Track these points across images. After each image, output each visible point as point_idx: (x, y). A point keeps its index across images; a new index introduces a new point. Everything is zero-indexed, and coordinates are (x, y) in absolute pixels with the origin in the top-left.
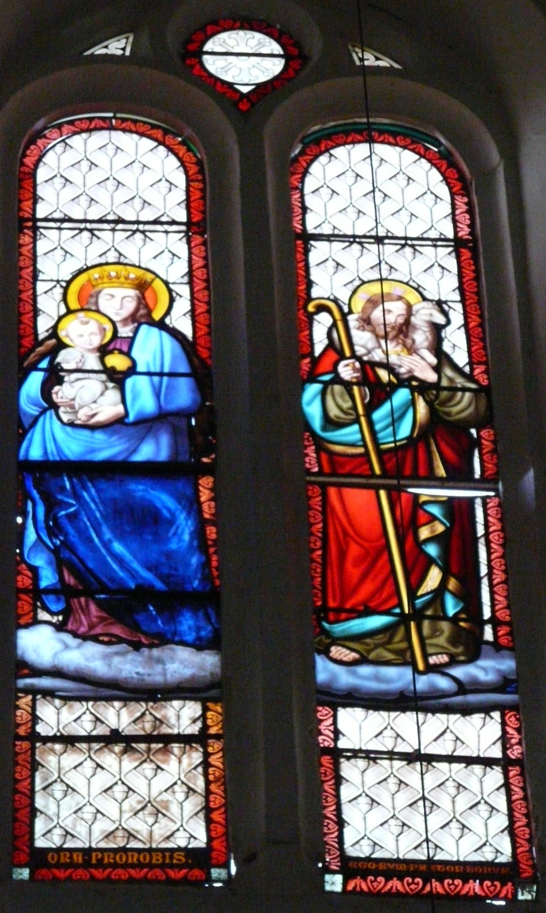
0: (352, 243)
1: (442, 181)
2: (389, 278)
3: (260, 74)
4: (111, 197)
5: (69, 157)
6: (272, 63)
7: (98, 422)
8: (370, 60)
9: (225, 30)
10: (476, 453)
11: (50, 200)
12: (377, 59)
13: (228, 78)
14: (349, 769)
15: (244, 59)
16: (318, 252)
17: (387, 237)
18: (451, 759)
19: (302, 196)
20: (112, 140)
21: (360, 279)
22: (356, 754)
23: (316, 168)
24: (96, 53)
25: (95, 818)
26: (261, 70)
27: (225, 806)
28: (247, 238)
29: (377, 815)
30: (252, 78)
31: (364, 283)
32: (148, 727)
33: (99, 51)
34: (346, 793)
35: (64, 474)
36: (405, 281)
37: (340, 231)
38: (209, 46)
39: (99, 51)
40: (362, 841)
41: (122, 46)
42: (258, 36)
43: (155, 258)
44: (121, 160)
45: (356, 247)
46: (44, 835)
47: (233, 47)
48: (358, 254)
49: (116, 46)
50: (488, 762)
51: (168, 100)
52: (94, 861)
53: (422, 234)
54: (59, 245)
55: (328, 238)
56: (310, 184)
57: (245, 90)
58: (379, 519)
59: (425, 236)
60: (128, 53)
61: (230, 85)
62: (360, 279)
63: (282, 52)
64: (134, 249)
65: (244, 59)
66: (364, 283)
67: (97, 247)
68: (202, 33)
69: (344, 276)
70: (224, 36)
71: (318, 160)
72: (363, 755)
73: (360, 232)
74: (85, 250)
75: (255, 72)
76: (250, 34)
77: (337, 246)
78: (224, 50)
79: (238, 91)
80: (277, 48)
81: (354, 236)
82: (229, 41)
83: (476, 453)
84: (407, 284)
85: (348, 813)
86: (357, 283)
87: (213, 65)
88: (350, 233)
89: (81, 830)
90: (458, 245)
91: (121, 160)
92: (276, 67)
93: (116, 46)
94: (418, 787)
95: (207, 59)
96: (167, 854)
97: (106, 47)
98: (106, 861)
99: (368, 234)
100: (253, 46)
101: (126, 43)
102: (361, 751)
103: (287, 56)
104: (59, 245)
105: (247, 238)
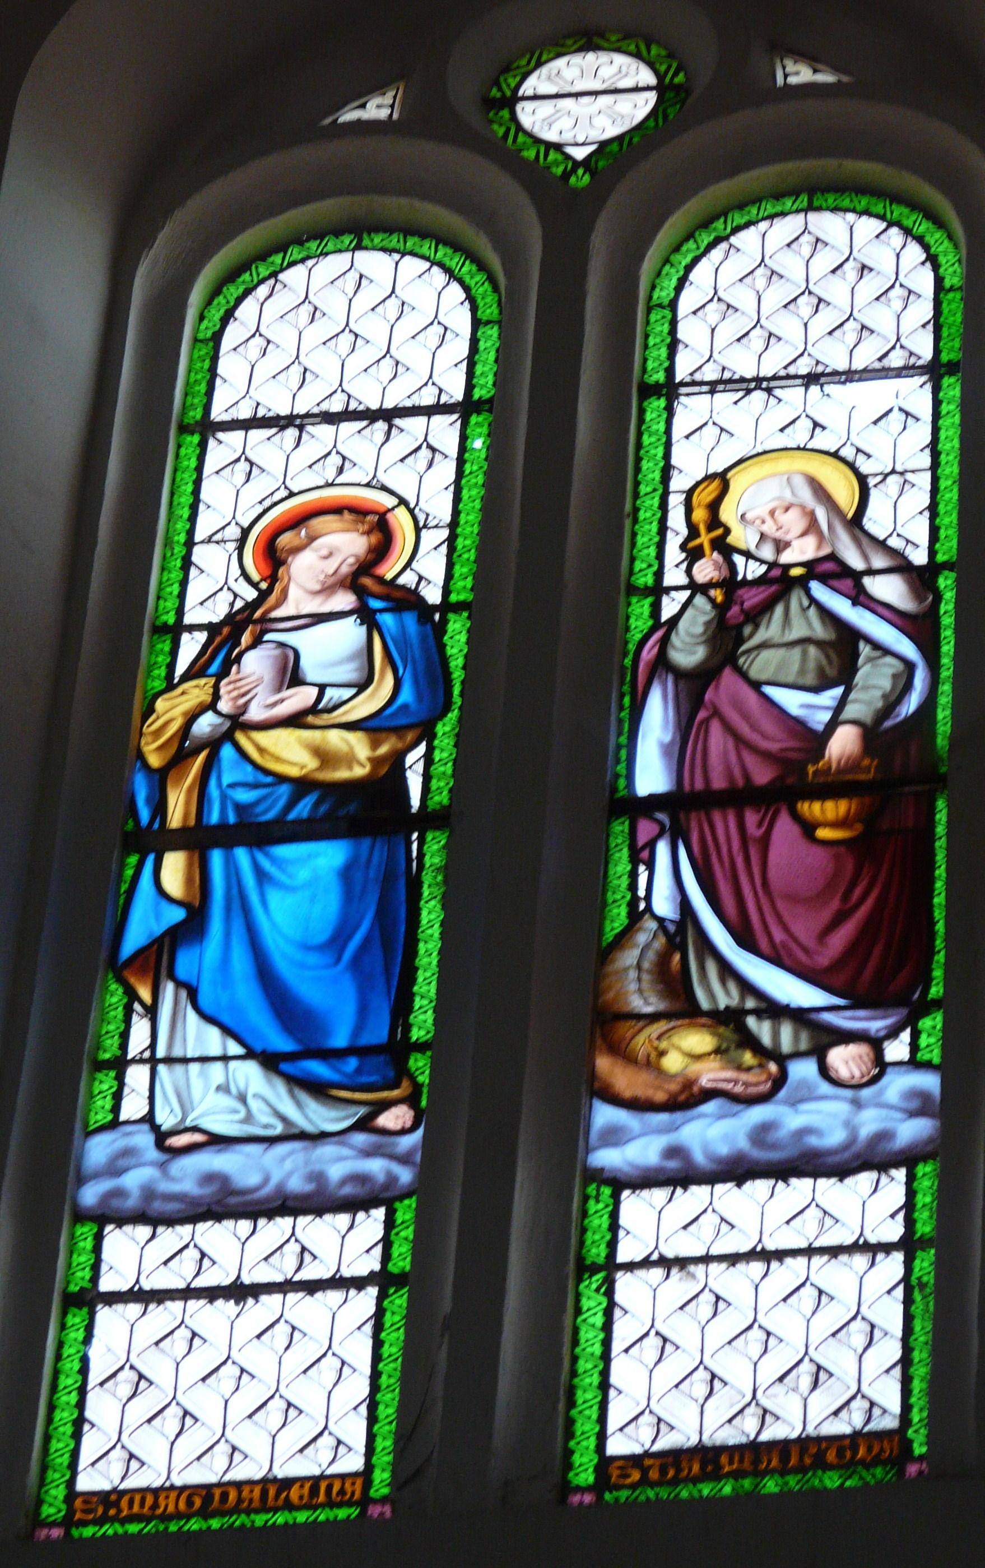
0: (748, 392)
1: (923, 263)
2: (338, 481)
4: (346, 369)
11: (702, 341)
12: (815, 71)
13: (551, 136)
15: (585, 102)
17: (721, 381)
19: (674, 323)
22: (359, 1283)
24: (341, 120)
33: (349, 116)
34: (623, 1331)
35: (414, 810)
37: (919, 358)
38: (528, 87)
39: (349, 116)
40: (853, 1325)
43: (875, 423)
45: (759, 396)
49: (377, 109)
51: (458, 187)
53: (692, 374)
55: (713, 387)
57: (579, 154)
59: (698, 377)
60: (395, 116)
67: (781, 414)
70: (561, 63)
76: (603, 57)
77: (724, 399)
78: (552, 90)
79: (568, 157)
80: (647, 77)
81: (758, 380)
84: (835, 455)
93: (377, 109)
99: (408, 403)
101: (395, 97)
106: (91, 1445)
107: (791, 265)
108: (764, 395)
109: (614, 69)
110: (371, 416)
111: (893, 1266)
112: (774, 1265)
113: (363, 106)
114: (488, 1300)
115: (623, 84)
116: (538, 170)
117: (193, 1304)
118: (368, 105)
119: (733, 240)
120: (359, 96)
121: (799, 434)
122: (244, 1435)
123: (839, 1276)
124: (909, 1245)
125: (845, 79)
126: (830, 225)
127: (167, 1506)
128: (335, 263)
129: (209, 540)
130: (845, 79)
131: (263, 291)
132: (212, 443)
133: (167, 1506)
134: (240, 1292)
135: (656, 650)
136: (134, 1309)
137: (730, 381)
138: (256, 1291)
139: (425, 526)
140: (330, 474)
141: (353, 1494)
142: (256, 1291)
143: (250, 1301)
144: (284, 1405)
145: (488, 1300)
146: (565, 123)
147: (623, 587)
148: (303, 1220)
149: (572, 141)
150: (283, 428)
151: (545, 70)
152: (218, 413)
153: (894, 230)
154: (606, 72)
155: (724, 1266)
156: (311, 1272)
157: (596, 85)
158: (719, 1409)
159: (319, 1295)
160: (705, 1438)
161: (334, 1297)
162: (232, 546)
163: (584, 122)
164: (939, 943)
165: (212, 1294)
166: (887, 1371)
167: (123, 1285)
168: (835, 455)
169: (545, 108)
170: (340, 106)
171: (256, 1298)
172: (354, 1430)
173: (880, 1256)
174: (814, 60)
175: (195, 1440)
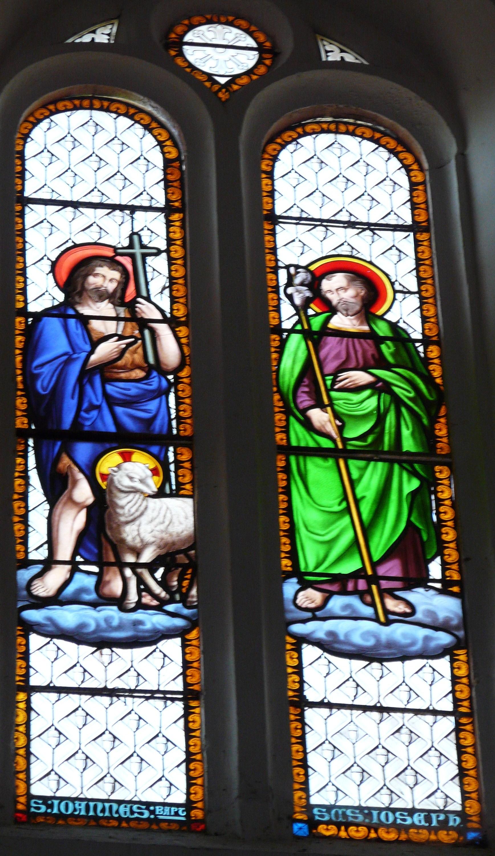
3: (235, 66)
6: (246, 57)
8: (335, 56)
9: (209, 22)
11: (287, 196)
15: (221, 52)
16: (33, 215)
17: (300, 219)
23: (37, 133)
26: (236, 63)
27: (205, 757)
29: (341, 763)
38: (189, 37)
39: (87, 39)
42: (235, 31)
44: (103, 137)
47: (211, 40)
48: (370, 240)
49: (102, 36)
50: (166, 696)
52: (427, 825)
56: (30, 149)
57: (223, 81)
61: (210, 77)
64: (368, 248)
65: (221, 52)
71: (39, 126)
72: (162, 696)
73: (373, 221)
75: (230, 64)
79: (217, 83)
80: (252, 43)
81: (369, 224)
82: (207, 34)
85: (312, 760)
86: (70, 244)
87: (192, 55)
88: (365, 221)
90: (168, 210)
91: (103, 137)
92: (248, 60)
93: (102, 36)
94: (378, 730)
95: (188, 50)
96: (92, 804)
97: (94, 32)
98: (451, 823)
102: (158, 691)
103: (260, 49)
107: (84, 136)
108: (324, 229)
110: (65, 204)
111: (449, 723)
112: (385, 715)
114: (245, 716)
116: (201, 83)
119: (299, 140)
120: (91, 25)
123: (150, 709)
124: (188, 695)
125: (365, 63)
128: (82, 115)
130: (365, 63)
135: (124, 346)
137: (306, 219)
141: (80, 810)
144: (84, 757)
145: (245, 716)
153: (137, 126)
155: (411, 715)
159: (368, 713)
165: (93, 692)
166: (178, 766)
167: (44, 683)
172: (180, 778)
174: (346, 45)
175: (93, 774)
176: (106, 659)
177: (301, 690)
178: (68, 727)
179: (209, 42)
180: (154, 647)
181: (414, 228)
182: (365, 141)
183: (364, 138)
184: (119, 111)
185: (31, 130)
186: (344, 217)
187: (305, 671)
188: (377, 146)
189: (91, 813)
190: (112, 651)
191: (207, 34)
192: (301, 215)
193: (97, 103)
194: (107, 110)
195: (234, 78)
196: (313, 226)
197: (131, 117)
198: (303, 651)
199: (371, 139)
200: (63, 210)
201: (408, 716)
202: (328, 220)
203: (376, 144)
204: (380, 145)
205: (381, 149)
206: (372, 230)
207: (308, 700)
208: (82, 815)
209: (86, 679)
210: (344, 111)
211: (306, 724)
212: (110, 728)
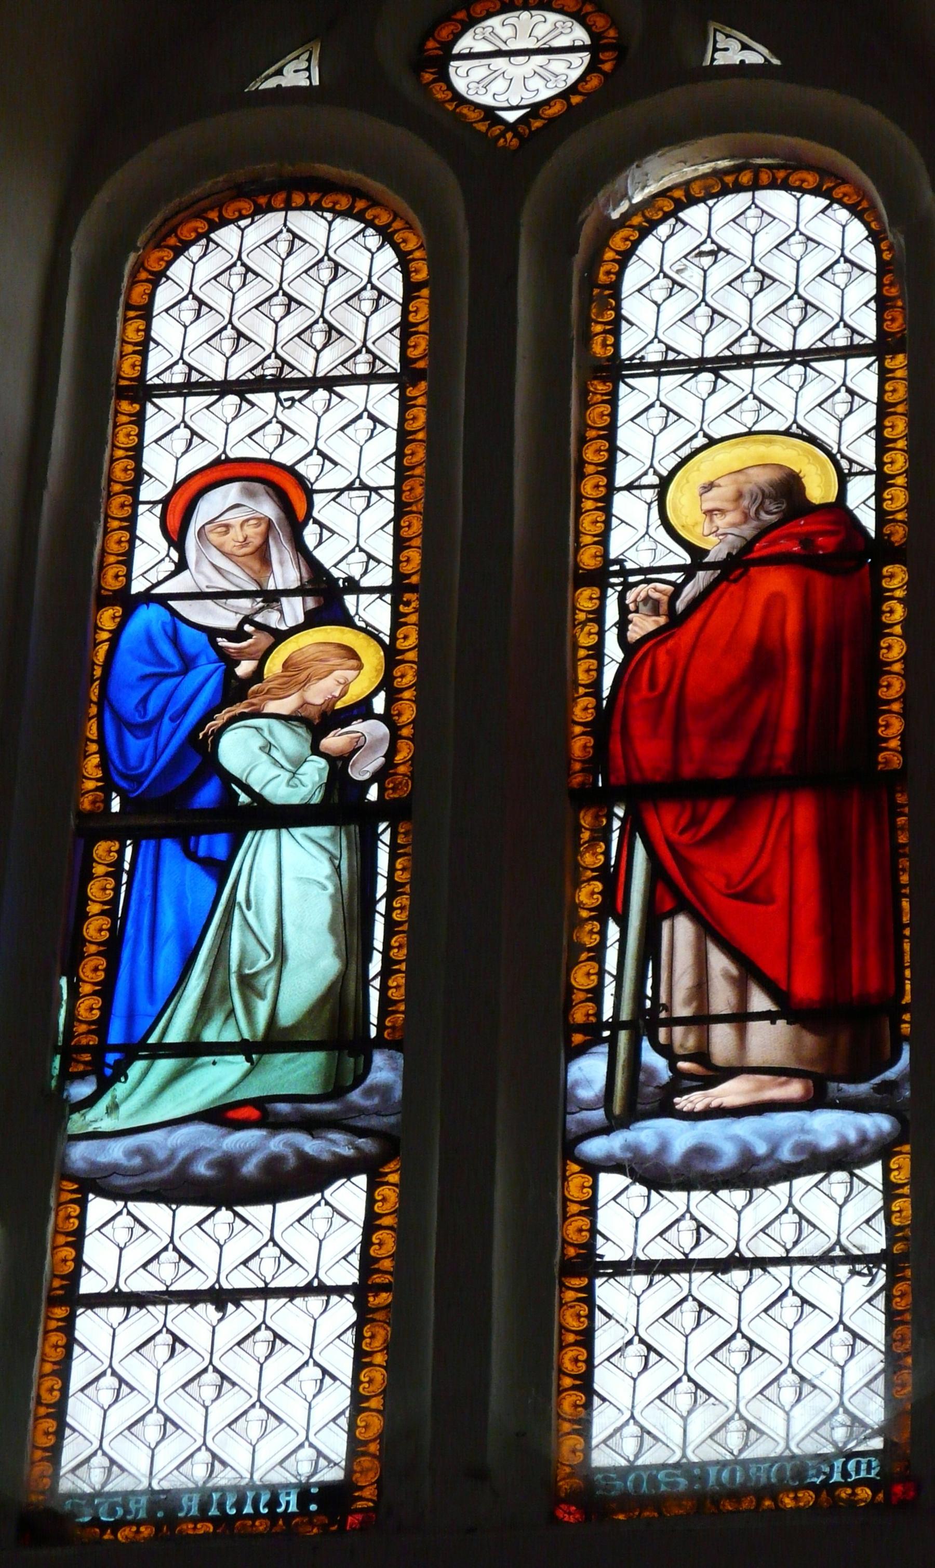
1: (866, 238)
4: (277, 350)
5: (685, 241)
7: (278, 1298)
10: (234, 786)
11: (649, 316)
12: (745, 47)
13: (486, 100)
14: (90, 1326)
15: (516, 67)
17: (665, 363)
18: (265, 1293)
20: (757, 201)
21: (706, 435)
25: (698, 1239)
28: (508, 393)
30: (526, 95)
31: (712, 441)
32: (687, 1240)
34: (606, 1339)
36: (782, 429)
38: (465, 44)
39: (271, 84)
41: (305, 65)
46: (82, 1390)
49: (297, 74)
54: (658, 399)
57: (511, 117)
58: (212, 899)
60: (316, 82)
62: (706, 435)
63: (588, 42)
66: (712, 441)
68: (575, 9)
69: (678, 433)
70: (495, 21)
74: (228, 429)
75: (535, 83)
76: (538, 15)
78: (488, 48)
79: (502, 121)
80: (580, 35)
82: (499, 30)
83: (234, 786)
84: (787, 433)
85: (603, 1379)
86: (700, 441)
87: (466, 78)
89: (670, 1429)
92: (571, 69)
93: (297, 74)
97: (279, 72)
99: (820, 345)
100: (540, 36)
104: (658, 399)
105: (508, 393)
106: (71, 1452)
109: (548, 27)
113: (279, 72)
114: (476, 1319)
115: (556, 43)
117: (174, 1309)
118: (285, 72)
120: (274, 57)
121: (747, 416)
122: (652, 1418)
123: (818, 1284)
124: (588, 1265)
126: (777, 201)
127: (288, 1503)
128: (271, 222)
129: (630, 487)
131: (663, 230)
132: (623, 389)
133: (288, 1503)
134: (221, 1298)
136: (116, 1313)
138: (237, 1296)
139: (851, 474)
140: (749, 419)
141: (189, 1509)
142: (237, 1296)
143: (231, 1307)
145: (476, 1319)
146: (499, 85)
147: (571, 575)
148: (697, 1195)
149: (506, 105)
150: (696, 373)
151: (478, 29)
152: (626, 351)
153: (370, 231)
154: (540, 31)
156: (711, 1250)
157: (531, 44)
158: (703, 1421)
159: (298, 1301)
160: (256, 1477)
161: (315, 1303)
162: (650, 494)
163: (517, 84)
164: (64, 1003)
165: (192, 1298)
168: (787, 433)
169: (479, 70)
170: (255, 75)
171: (238, 1305)
173: (334, 1299)
176: (840, 1192)
177: (590, 1246)
178: (138, 1371)
179: (504, 48)
180: (318, 1196)
181: (881, 348)
182: (807, 197)
183: (804, 192)
184: (337, 207)
185: (169, 264)
186: (747, 347)
187: (88, 1242)
188: (827, 202)
189: (248, 1509)
190: (852, 1175)
191: (506, 33)
192: (759, 349)
193: (298, 199)
194: (317, 208)
195: (535, 109)
196: (782, 367)
197: (359, 217)
198: (90, 1205)
199: (816, 192)
200: (219, 404)
201: (799, 1270)
202: (717, 357)
203: (826, 198)
204: (833, 201)
205: (836, 206)
206: (805, 364)
207: (882, 1250)
208: (292, 1513)
209: (703, 1238)
210: (768, 147)
211: (76, 1340)
212: (212, 1353)
